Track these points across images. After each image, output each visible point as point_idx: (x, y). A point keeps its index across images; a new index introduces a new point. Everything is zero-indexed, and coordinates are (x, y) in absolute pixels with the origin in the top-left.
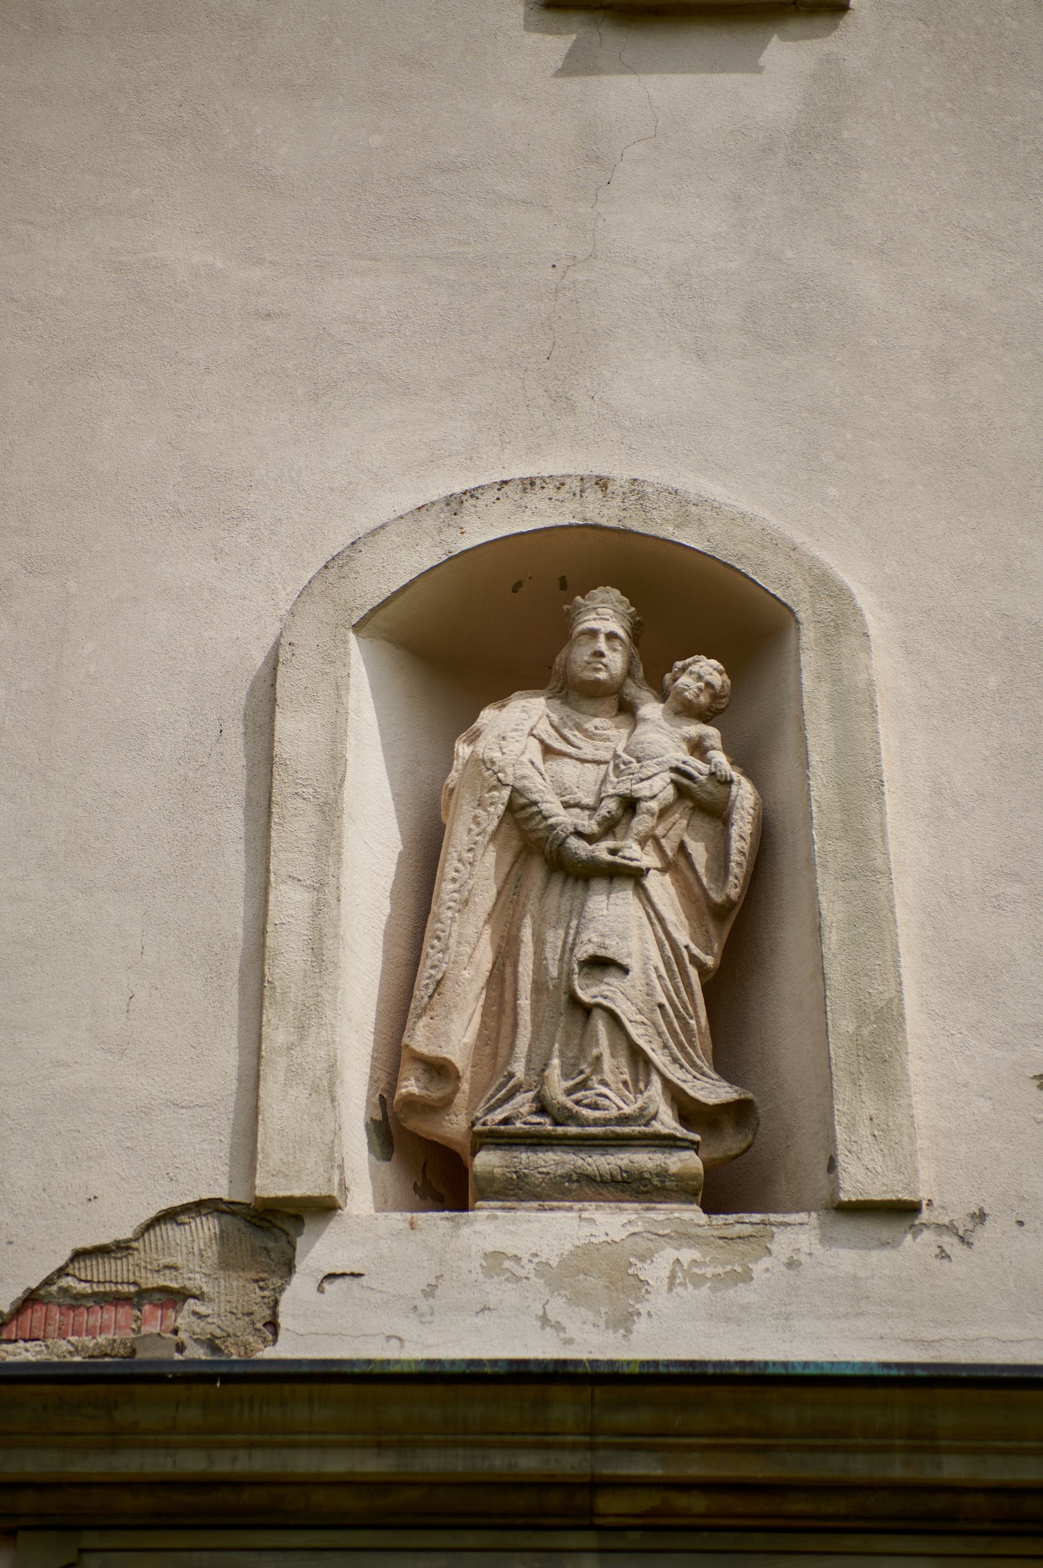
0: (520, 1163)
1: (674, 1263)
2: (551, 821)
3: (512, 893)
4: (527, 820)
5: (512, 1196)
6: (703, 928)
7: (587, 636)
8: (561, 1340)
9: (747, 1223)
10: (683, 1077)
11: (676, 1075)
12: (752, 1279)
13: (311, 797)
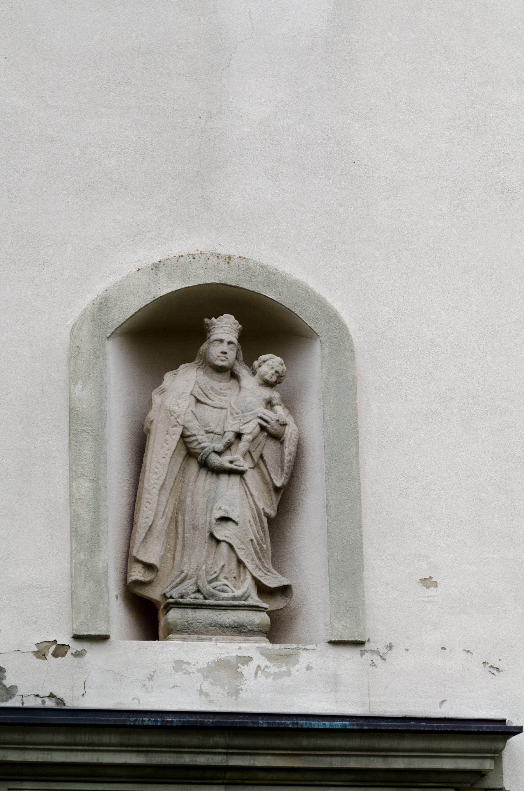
0: (189, 617)
1: (257, 667)
2: (203, 445)
3: (181, 477)
4: (190, 443)
5: (184, 632)
6: (270, 497)
7: (218, 342)
8: (208, 700)
9: (289, 649)
10: (261, 575)
11: (258, 574)
12: (291, 674)
13: (90, 432)
